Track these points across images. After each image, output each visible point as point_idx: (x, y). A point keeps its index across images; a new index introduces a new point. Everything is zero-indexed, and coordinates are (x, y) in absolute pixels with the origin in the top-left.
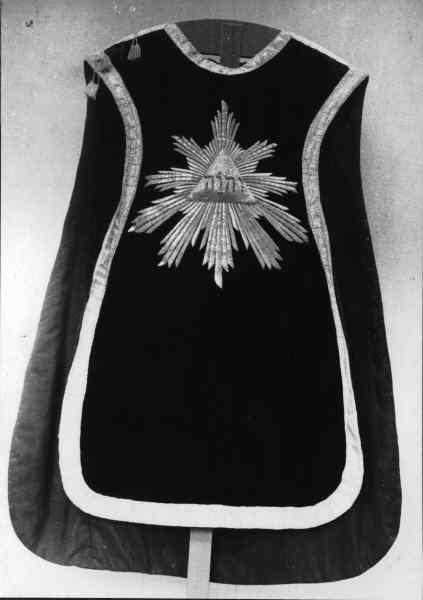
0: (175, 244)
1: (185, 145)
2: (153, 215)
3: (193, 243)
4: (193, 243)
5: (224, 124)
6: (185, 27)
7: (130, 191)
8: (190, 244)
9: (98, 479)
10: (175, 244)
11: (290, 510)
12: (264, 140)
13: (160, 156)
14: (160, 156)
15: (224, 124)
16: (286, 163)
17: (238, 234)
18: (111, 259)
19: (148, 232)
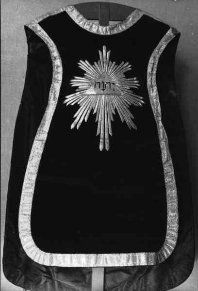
0: (81, 116)
1: (84, 65)
2: (70, 99)
3: (114, 113)
4: (114, 113)
5: (105, 54)
6: (80, 8)
7: (57, 86)
8: (113, 114)
9: (44, 243)
10: (81, 116)
11: (52, 115)
12: (68, 105)
13: (72, 71)
14: (72, 71)
15: (105, 54)
16: (139, 71)
17: (116, 110)
18: (30, 159)
19: (72, 104)
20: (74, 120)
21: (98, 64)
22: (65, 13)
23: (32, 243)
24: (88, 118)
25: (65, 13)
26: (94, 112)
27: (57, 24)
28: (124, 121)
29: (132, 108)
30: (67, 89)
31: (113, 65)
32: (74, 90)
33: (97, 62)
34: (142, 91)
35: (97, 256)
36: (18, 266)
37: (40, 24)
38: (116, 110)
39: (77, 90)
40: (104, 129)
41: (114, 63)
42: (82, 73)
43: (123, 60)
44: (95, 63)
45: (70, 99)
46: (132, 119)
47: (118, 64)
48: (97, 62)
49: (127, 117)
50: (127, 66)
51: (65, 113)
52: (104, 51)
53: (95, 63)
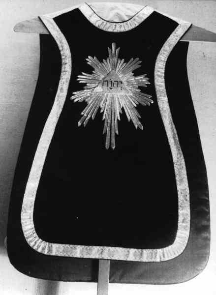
0: (87, 114)
1: (90, 60)
2: (78, 97)
10: (87, 114)
16: (147, 69)
20: (133, 123)
21: (106, 61)
22: (77, 11)
23: (159, 251)
24: (96, 116)
25: (155, 13)
26: (102, 111)
27: (72, 22)
28: (131, 120)
29: (139, 108)
30: (75, 86)
31: (106, 63)
32: (82, 87)
33: (106, 60)
34: (149, 90)
35: (37, 249)
36: (25, 261)
37: (59, 20)
38: (123, 109)
39: (85, 88)
40: (111, 129)
41: (123, 60)
42: (90, 70)
43: (139, 58)
44: (104, 60)
45: (78, 97)
46: (139, 118)
47: (126, 61)
48: (106, 60)
49: (132, 115)
50: (135, 63)
51: (72, 109)
52: (113, 47)
53: (104, 60)
